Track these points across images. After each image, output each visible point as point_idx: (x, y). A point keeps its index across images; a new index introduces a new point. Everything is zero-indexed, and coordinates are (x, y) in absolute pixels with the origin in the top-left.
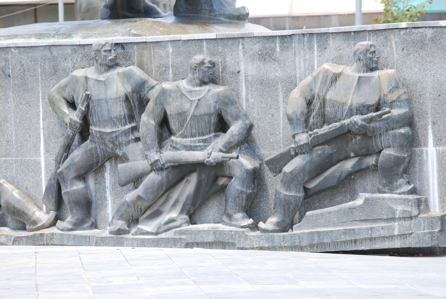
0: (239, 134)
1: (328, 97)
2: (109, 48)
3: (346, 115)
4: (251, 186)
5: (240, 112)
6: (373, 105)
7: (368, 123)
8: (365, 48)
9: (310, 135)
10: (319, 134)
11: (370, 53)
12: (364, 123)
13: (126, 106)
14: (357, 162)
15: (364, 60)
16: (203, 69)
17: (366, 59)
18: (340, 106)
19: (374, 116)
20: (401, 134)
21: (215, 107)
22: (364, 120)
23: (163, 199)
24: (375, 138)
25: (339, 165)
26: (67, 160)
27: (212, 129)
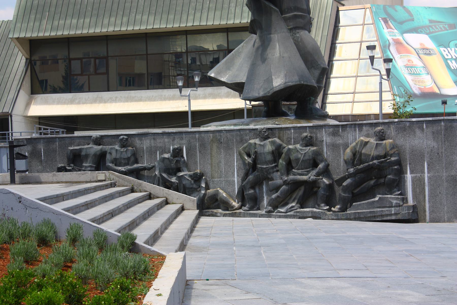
23: (289, 197)
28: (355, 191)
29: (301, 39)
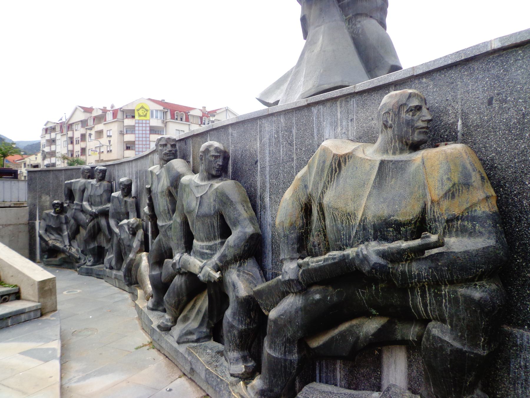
0: (235, 245)
1: (326, 201)
2: (164, 143)
3: (355, 237)
4: (245, 320)
5: (240, 215)
6: (409, 223)
7: (392, 261)
8: (396, 100)
9: (300, 266)
10: (310, 267)
11: (407, 112)
12: (382, 261)
13: (170, 200)
14: (383, 326)
15: (395, 126)
16: (208, 159)
17: (399, 125)
18: (344, 218)
19: (404, 250)
20: (469, 300)
21: (215, 207)
22: (383, 255)
23: (192, 303)
24: (413, 294)
25: (354, 322)
26: (327, 218)
27: (217, 234)
28: (316, 343)
29: (363, 30)
